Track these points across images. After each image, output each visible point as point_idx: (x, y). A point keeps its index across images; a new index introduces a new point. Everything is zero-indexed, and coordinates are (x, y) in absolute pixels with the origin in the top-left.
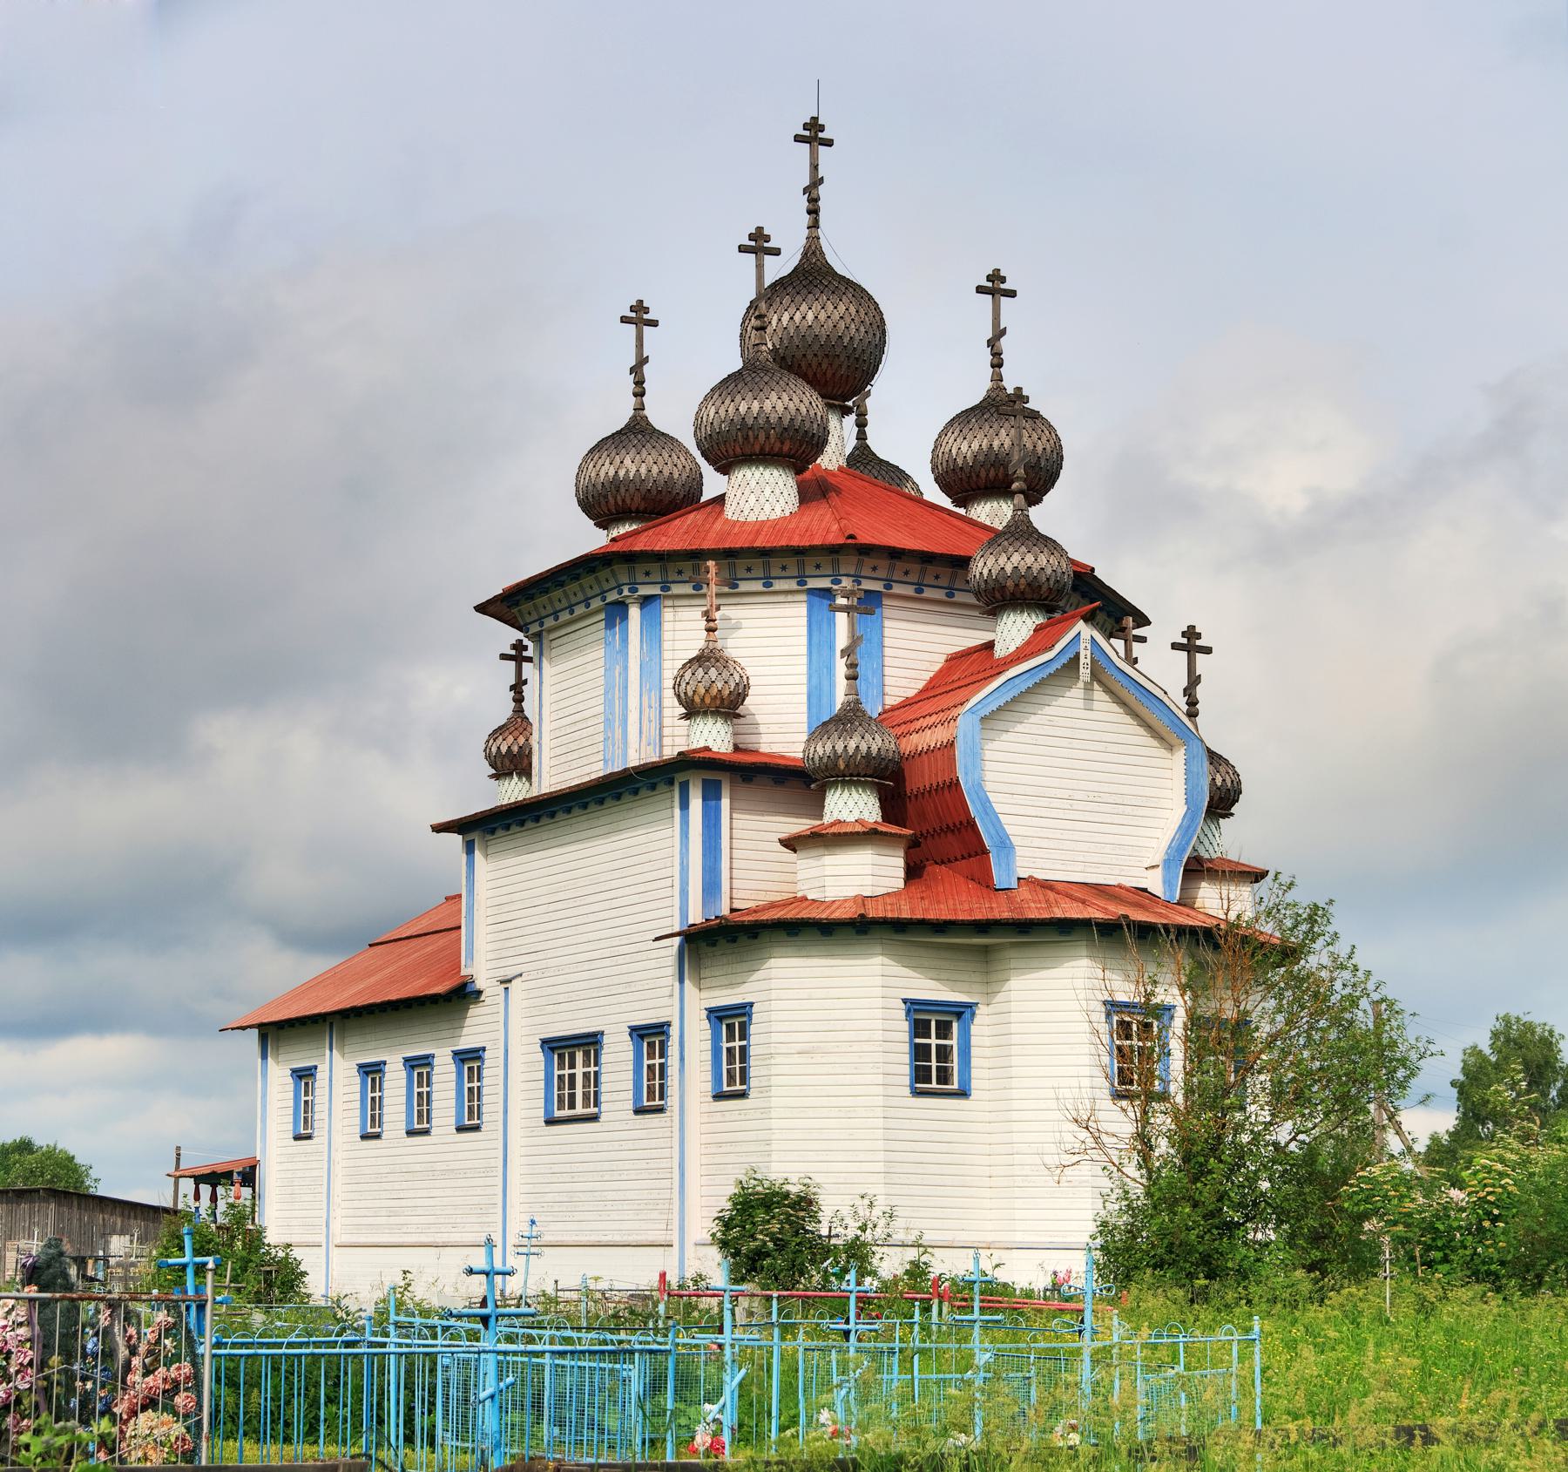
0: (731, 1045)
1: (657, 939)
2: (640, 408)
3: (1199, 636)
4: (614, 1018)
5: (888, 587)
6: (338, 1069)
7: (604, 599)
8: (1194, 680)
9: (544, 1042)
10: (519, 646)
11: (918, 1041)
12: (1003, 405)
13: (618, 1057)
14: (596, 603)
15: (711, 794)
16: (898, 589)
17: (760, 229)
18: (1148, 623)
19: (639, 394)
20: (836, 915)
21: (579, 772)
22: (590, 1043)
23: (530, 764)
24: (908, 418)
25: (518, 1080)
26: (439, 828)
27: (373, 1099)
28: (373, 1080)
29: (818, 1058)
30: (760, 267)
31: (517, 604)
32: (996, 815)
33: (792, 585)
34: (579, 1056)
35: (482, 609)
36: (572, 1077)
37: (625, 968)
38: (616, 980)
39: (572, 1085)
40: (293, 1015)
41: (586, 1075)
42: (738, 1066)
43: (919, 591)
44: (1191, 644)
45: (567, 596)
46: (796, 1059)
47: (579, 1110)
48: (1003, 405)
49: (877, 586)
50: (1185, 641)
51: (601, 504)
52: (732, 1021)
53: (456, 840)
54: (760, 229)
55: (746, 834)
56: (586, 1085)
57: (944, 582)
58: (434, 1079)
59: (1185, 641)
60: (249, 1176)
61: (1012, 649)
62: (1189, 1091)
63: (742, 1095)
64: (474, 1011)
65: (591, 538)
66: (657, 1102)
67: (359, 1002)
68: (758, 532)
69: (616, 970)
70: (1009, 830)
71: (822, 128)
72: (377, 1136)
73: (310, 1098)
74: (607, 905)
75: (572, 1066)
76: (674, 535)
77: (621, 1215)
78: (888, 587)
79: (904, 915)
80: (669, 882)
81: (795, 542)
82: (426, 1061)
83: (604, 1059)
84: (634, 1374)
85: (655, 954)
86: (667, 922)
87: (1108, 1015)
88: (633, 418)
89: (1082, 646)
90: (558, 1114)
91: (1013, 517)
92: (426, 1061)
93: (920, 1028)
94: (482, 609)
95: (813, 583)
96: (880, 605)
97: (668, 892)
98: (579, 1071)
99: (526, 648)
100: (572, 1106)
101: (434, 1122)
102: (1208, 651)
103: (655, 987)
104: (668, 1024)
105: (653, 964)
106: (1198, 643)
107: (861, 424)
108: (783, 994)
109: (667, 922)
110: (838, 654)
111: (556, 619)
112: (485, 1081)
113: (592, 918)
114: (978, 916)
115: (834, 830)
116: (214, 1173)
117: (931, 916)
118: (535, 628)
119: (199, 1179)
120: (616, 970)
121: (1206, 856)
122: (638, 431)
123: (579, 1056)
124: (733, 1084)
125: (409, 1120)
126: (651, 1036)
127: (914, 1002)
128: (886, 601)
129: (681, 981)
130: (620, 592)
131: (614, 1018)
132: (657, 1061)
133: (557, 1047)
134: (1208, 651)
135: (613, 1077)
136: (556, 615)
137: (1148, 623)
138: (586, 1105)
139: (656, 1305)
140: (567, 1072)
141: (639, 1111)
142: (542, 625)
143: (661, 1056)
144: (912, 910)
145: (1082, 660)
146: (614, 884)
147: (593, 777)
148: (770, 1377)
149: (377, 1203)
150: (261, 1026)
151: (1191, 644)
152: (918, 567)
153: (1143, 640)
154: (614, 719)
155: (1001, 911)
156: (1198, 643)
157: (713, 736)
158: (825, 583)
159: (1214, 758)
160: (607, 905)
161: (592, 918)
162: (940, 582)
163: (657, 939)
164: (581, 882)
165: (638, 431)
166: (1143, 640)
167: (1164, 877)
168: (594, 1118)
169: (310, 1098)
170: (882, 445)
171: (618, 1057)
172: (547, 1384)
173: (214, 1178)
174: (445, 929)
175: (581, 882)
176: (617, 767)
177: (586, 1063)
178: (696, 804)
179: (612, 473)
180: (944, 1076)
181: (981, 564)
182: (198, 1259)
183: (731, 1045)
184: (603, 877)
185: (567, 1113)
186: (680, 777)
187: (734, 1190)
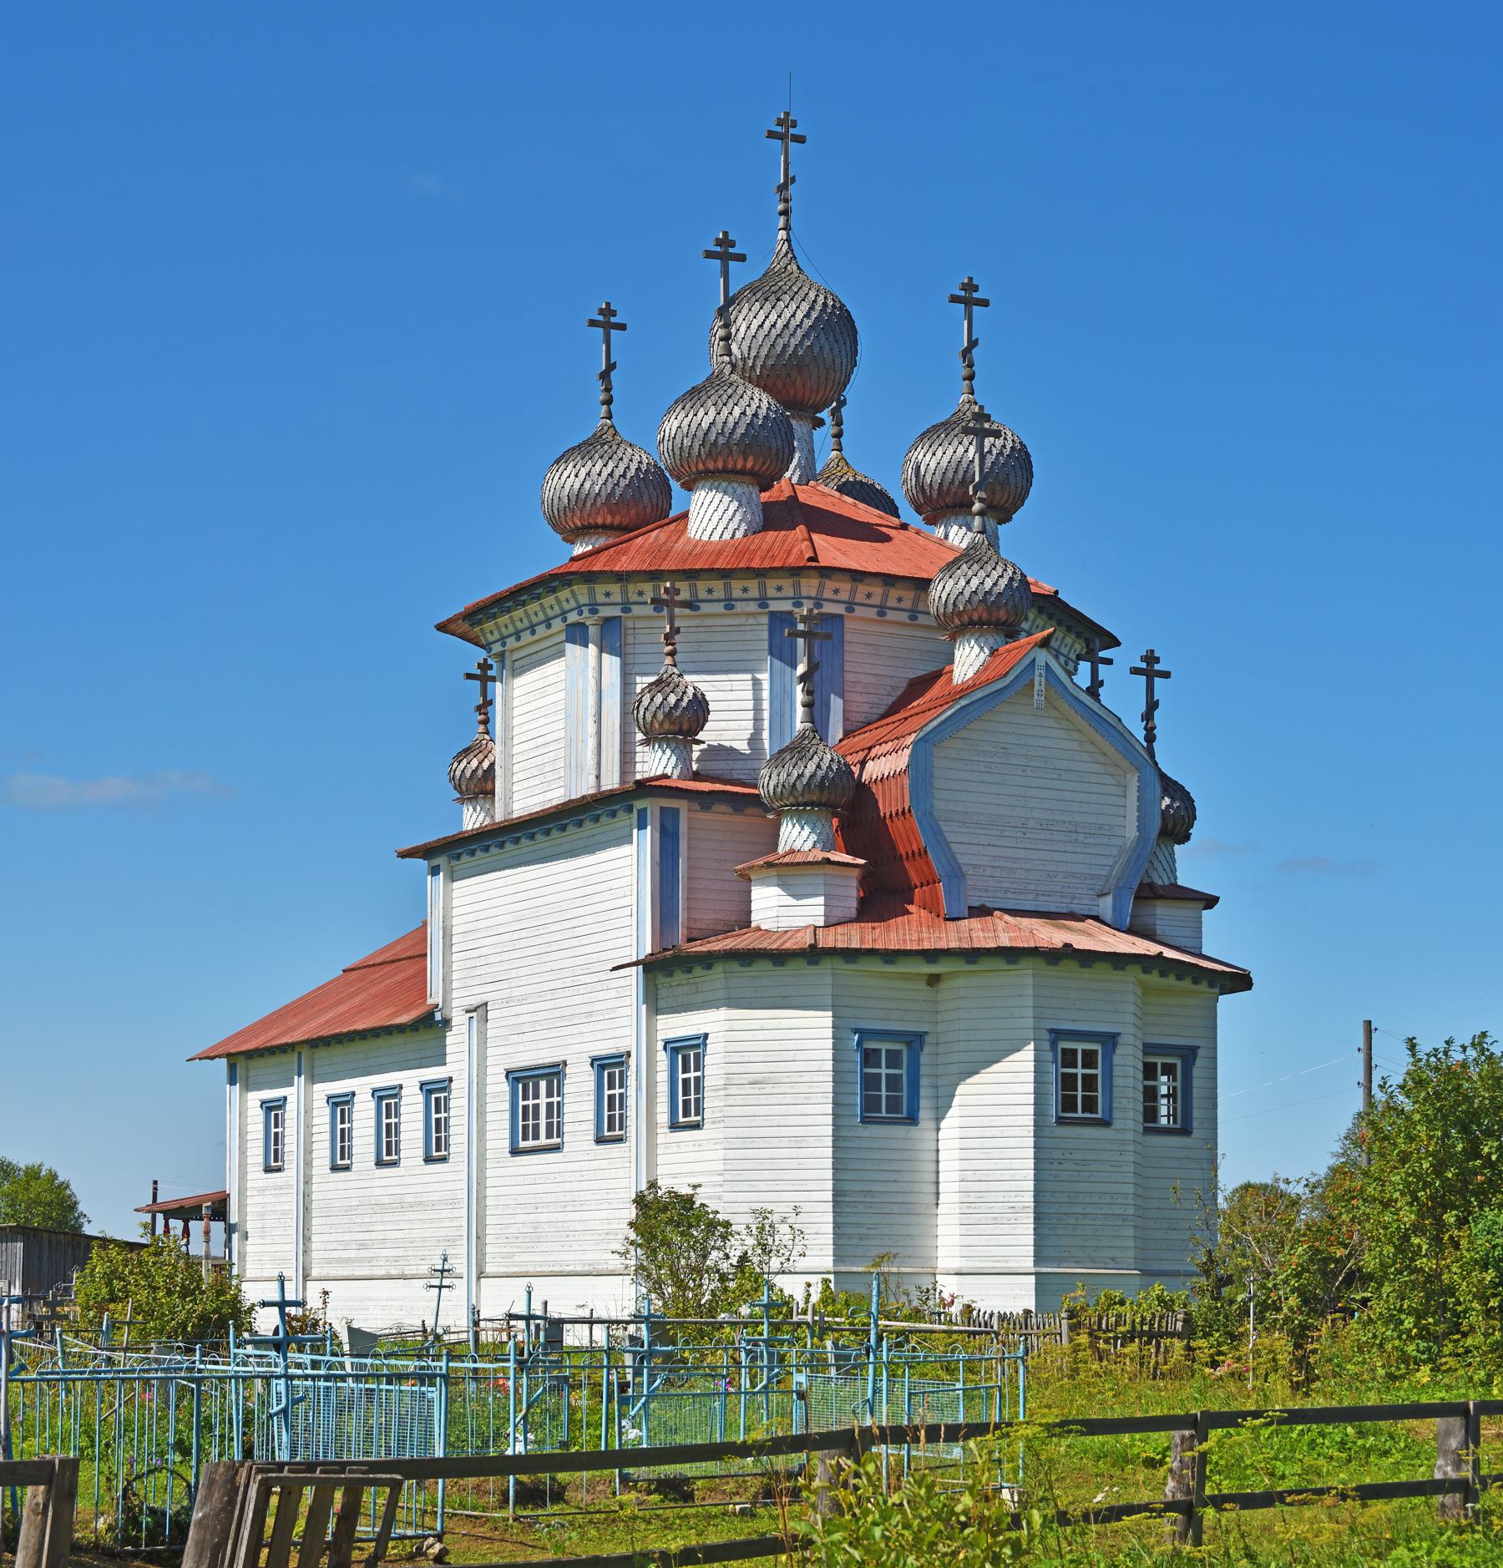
0: (686, 1076)
1: (615, 969)
3: (1157, 660)
4: (577, 1048)
5: (850, 610)
6: (306, 1100)
7: (564, 620)
8: (1152, 705)
9: (594, 1060)
10: (484, 666)
13: (580, 1088)
18: (1117, 643)
20: (787, 946)
21: (540, 798)
22: (554, 1073)
25: (483, 1112)
26: (403, 855)
27: (388, 1125)
28: (343, 1111)
29: (768, 1089)
30: (725, 274)
31: (480, 623)
32: (947, 843)
34: (543, 1084)
35: (442, 628)
37: (586, 998)
38: (578, 1010)
39: (536, 1116)
41: (550, 1106)
42: (692, 1097)
44: (1150, 669)
45: (559, 602)
46: (748, 1089)
47: (543, 1140)
50: (1144, 665)
52: (686, 1052)
53: (422, 864)
56: (549, 1115)
58: (403, 1110)
59: (1144, 665)
60: (220, 1209)
61: (970, 674)
63: (697, 1126)
66: (617, 1133)
67: (326, 1032)
68: (719, 553)
69: (578, 1000)
70: (962, 860)
71: (794, 124)
72: (347, 1168)
73: (280, 1130)
74: (569, 934)
75: (536, 1096)
77: (557, 1248)
79: (854, 945)
80: (627, 911)
81: (755, 564)
82: (396, 1091)
83: (567, 1089)
84: (435, 1395)
85: (615, 984)
86: (627, 951)
87: (1053, 1045)
89: (1037, 673)
90: (523, 1144)
92: (396, 1091)
94: (442, 628)
95: (775, 606)
97: (627, 921)
98: (543, 1101)
99: (490, 667)
100: (536, 1137)
101: (402, 1154)
102: (1166, 675)
103: (617, 1017)
104: (629, 1054)
105: (612, 994)
106: (1157, 667)
109: (627, 951)
110: (796, 680)
111: (518, 639)
112: (452, 1112)
113: (555, 947)
114: (926, 946)
115: (787, 860)
116: (182, 1207)
117: (879, 946)
118: (497, 648)
119: (169, 1214)
120: (578, 1000)
121: (1160, 882)
123: (543, 1084)
124: (687, 1113)
125: (599, 1127)
126: (609, 1067)
130: (580, 614)
131: (577, 1048)
132: (617, 1091)
133: (522, 1079)
134: (1166, 675)
135: (575, 1107)
137: (1117, 643)
138: (549, 1135)
140: (531, 1102)
141: (600, 1140)
142: (504, 645)
143: (621, 1087)
144: (862, 941)
145: (1037, 687)
146: (576, 912)
147: (554, 803)
149: (347, 1237)
150: (229, 1056)
151: (1150, 669)
153: (1109, 662)
156: (1157, 667)
159: (1170, 786)
160: (569, 934)
161: (555, 947)
163: (615, 969)
164: (543, 911)
166: (1109, 662)
168: (556, 1148)
169: (280, 1130)
171: (580, 1088)
173: (186, 1212)
174: (409, 958)
175: (543, 911)
177: (550, 1094)
179: (577, 486)
180: (893, 1104)
181: (940, 588)
183: (686, 1076)
184: (565, 905)
185: (530, 1143)
186: (639, 804)
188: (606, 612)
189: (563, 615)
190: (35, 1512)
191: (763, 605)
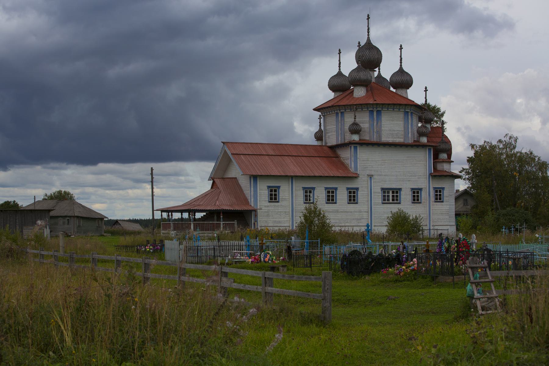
2: (340, 69)
12: (401, 71)
15: (355, 148)
16: (384, 109)
24: (387, 70)
33: (366, 109)
34: (391, 192)
36: (388, 196)
48: (401, 71)
49: (380, 109)
51: (333, 87)
62: (397, 241)
76: (243, 265)
93: (414, 193)
95: (370, 109)
100: (388, 200)
107: (379, 69)
122: (340, 74)
139: (437, 122)
154: (337, 138)
155: (350, 175)
157: (356, 138)
158: (372, 109)
165: (340, 74)
167: (305, 146)
170: (384, 75)
172: (195, 279)
176: (243, 189)
178: (410, 117)
182: (172, 225)
188: (342, 111)
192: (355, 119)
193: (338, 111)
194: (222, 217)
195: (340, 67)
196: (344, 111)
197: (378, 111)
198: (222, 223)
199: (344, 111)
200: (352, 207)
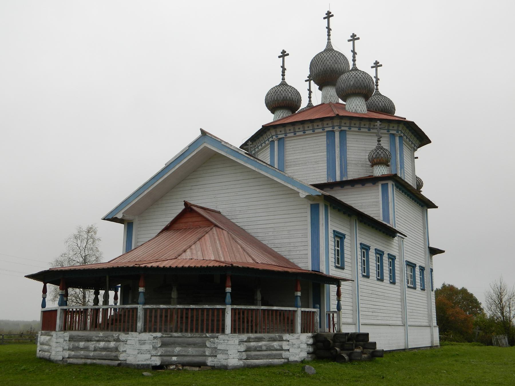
2: (310, 101)
5: (286, 135)
11: (89, 328)
14: (267, 142)
17: (353, 34)
19: (283, 75)
23: (146, 365)
40: (366, 213)
43: (314, 131)
54: (353, 34)
55: (364, 305)
57: (367, 126)
64: (307, 73)
65: (269, 118)
71: (379, 63)
78: (286, 135)
88: (309, 104)
91: (171, 294)
95: (327, 129)
96: (394, 237)
108: (352, 148)
127: (408, 262)
128: (347, 133)
129: (376, 77)
136: (258, 148)
148: (260, 173)
152: (368, 123)
157: (380, 171)
160: (411, 251)
162: (310, 128)
187: (511, 347)
188: (343, 128)
189: (268, 140)
190: (116, 356)
191: (388, 131)
192: (379, 141)
193: (336, 128)
194: (229, 290)
195: (283, 75)
196: (346, 129)
197: (341, 132)
198: (229, 308)
199: (346, 129)
200: (380, 283)
